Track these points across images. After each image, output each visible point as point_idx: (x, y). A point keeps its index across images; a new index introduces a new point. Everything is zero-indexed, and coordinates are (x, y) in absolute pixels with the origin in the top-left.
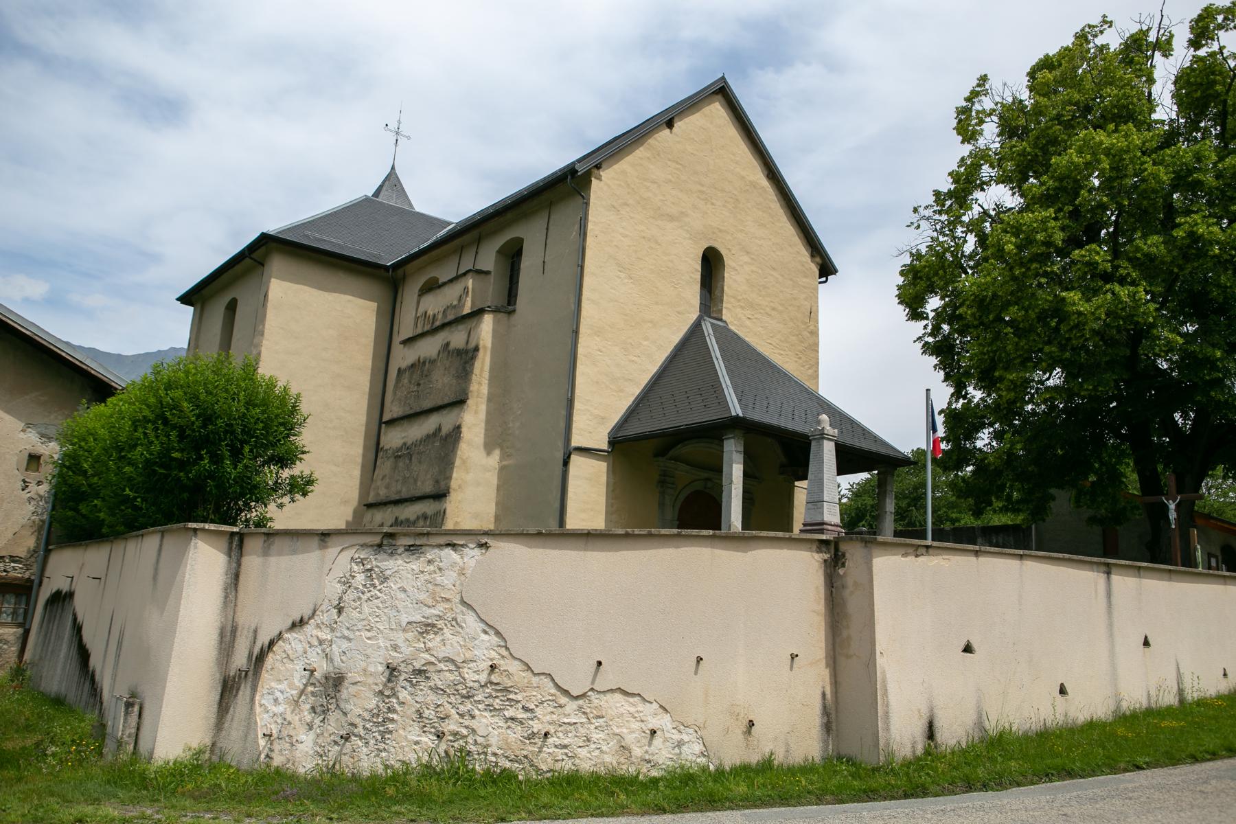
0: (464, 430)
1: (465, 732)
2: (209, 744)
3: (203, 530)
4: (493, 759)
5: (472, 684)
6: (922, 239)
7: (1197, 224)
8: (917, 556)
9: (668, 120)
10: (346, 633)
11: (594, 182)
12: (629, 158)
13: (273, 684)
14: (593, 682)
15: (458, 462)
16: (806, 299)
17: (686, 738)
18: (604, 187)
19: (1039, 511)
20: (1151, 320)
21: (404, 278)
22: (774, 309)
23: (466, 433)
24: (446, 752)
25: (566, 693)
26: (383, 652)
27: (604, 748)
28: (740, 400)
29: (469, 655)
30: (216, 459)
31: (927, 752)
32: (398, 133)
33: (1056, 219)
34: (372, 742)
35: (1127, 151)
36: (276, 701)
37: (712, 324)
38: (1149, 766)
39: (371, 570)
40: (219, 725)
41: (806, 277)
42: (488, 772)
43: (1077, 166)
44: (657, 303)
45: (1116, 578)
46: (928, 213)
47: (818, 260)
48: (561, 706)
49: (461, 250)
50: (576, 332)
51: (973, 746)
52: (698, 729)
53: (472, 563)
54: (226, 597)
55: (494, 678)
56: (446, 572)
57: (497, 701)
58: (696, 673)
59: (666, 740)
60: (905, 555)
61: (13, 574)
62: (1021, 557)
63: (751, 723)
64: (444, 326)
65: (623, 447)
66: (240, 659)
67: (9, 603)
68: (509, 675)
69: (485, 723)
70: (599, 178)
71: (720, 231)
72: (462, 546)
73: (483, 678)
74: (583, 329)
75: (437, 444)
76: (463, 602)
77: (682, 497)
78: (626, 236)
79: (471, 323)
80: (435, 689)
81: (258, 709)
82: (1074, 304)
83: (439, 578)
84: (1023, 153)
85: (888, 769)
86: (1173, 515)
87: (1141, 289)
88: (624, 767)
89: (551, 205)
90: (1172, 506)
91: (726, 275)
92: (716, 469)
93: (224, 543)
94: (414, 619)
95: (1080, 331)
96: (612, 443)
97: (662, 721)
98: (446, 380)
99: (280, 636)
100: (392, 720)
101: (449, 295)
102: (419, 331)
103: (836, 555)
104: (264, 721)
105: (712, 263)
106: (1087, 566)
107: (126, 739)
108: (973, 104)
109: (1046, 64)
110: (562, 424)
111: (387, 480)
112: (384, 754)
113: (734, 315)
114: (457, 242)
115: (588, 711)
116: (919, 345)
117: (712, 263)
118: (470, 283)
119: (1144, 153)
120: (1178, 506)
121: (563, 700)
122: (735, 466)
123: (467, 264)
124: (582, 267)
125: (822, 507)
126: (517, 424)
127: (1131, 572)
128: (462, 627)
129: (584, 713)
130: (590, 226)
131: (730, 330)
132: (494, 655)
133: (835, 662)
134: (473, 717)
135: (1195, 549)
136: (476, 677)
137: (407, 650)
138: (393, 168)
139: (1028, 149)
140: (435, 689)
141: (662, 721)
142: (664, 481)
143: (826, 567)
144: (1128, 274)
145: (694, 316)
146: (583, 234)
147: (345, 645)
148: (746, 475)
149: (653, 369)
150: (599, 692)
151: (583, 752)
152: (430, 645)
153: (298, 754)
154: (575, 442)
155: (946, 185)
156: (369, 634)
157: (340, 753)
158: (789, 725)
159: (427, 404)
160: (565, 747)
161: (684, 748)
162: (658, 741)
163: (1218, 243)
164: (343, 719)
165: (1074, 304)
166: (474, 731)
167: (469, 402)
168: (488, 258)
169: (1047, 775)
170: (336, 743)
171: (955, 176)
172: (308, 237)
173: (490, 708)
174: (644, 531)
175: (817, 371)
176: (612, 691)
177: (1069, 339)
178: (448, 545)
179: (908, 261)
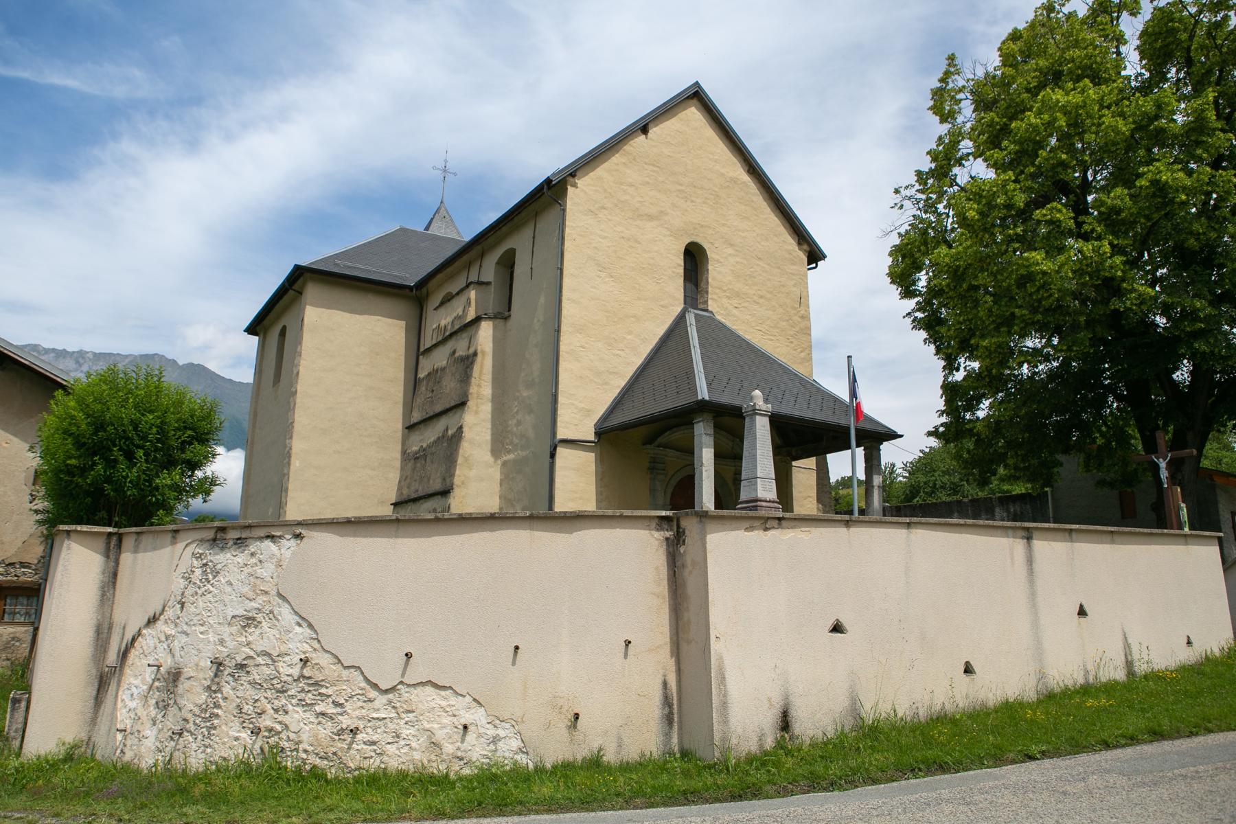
0: (465, 429)
1: (278, 727)
2: (85, 738)
3: (76, 531)
4: (304, 756)
5: (286, 678)
6: (904, 219)
7: (1160, 172)
8: (766, 529)
9: (643, 127)
10: (185, 628)
12: (606, 165)
13: (132, 680)
14: (403, 676)
15: (460, 460)
16: (794, 285)
17: (502, 733)
18: (577, 196)
19: (1043, 474)
20: (1119, 273)
21: (428, 295)
23: (467, 433)
24: (262, 749)
25: (375, 686)
26: (211, 647)
27: (414, 745)
28: (709, 385)
29: (283, 648)
30: (111, 464)
31: (780, 745)
33: (1015, 181)
34: (200, 737)
35: (1084, 106)
36: (132, 694)
37: (696, 315)
38: (1044, 755)
39: (205, 565)
40: (94, 721)
42: (298, 770)
43: (1035, 128)
44: (639, 299)
45: (1039, 545)
46: (908, 193)
47: (805, 247)
48: (370, 701)
49: (469, 265)
50: (558, 331)
51: (842, 736)
52: (515, 723)
53: (288, 554)
54: (103, 595)
55: (306, 672)
56: (266, 565)
57: (310, 695)
58: (514, 664)
59: (480, 736)
60: (751, 529)
61: (23, 578)
62: (909, 525)
63: (577, 716)
66: (112, 658)
67: (22, 604)
68: (321, 668)
69: (297, 718)
70: (575, 185)
72: (280, 537)
73: (296, 671)
74: (564, 328)
76: (280, 595)
77: (674, 482)
78: (605, 238)
79: (470, 331)
80: (253, 683)
81: (120, 704)
82: (1038, 264)
83: (259, 571)
84: (991, 124)
85: (721, 767)
86: (1164, 474)
87: (1106, 243)
88: (435, 765)
89: (536, 215)
90: (1163, 464)
92: (689, 451)
93: (101, 543)
94: (237, 613)
95: (1047, 291)
96: (603, 432)
97: (477, 716)
98: (453, 385)
99: (139, 633)
100: (217, 716)
101: (456, 308)
102: (434, 342)
103: (678, 532)
104: (123, 719)
105: (694, 258)
106: (999, 532)
107: (12, 734)
108: (947, 84)
109: (1015, 36)
112: (209, 750)
113: (719, 304)
114: (465, 258)
115: (398, 705)
116: (909, 320)
117: (694, 258)
118: (473, 294)
119: (1102, 107)
120: (1169, 465)
121: (373, 694)
122: (704, 450)
124: (561, 270)
126: (515, 421)
127: (1060, 535)
128: (277, 620)
129: (394, 707)
130: (567, 231)
131: (715, 320)
132: (306, 647)
133: (678, 648)
134: (287, 713)
135: (1179, 508)
136: (290, 671)
137: (231, 644)
139: (997, 119)
140: (253, 683)
141: (477, 716)
143: (668, 545)
144: (1093, 230)
145: (679, 308)
147: (184, 639)
148: (717, 456)
149: (638, 361)
150: (409, 686)
151: (391, 749)
152: (250, 638)
153: (143, 749)
154: (560, 436)
155: (927, 165)
156: (202, 629)
157: (175, 749)
158: (621, 714)
159: (438, 409)
160: (374, 743)
161: (500, 744)
162: (471, 737)
163: (1184, 188)
164: (179, 714)
165: (1038, 264)
166: (287, 727)
168: (489, 269)
169: (913, 770)
170: (172, 739)
171: (934, 155)
172: (338, 265)
173: (303, 704)
174: (618, 513)
176: (421, 684)
177: (1040, 301)
178: (268, 537)
179: (897, 241)
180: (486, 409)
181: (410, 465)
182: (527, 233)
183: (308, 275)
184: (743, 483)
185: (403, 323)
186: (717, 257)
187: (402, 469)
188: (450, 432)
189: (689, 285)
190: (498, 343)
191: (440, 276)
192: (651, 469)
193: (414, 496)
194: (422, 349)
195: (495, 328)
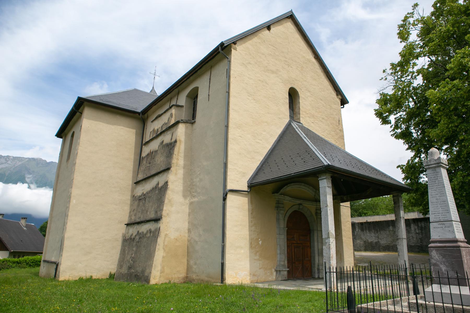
0: (169, 183)
11: (233, 51)
12: (250, 42)
15: (166, 201)
16: (336, 115)
18: (237, 54)
21: (148, 117)
22: (323, 119)
23: (170, 185)
32: (155, 75)
41: (335, 104)
47: (340, 97)
49: (171, 99)
50: (227, 127)
64: (161, 133)
65: (256, 188)
70: (235, 49)
71: (296, 80)
74: (231, 125)
75: (157, 192)
77: (288, 215)
78: (251, 79)
89: (211, 67)
91: (300, 101)
101: (164, 119)
102: (151, 138)
105: (293, 95)
110: (222, 177)
111: (135, 212)
114: (169, 96)
117: (293, 95)
123: (174, 102)
124: (228, 93)
126: (198, 179)
130: (232, 72)
138: (153, 88)
142: (279, 206)
146: (229, 77)
149: (269, 146)
159: (153, 172)
167: (172, 169)
168: (182, 100)
180: (181, 172)
181: (136, 203)
182: (205, 78)
183: (85, 103)
184: (432, 225)
185: (135, 130)
187: (131, 205)
188: (160, 186)
190: (189, 136)
191: (154, 107)
192: (277, 207)
193: (138, 220)
194: (144, 142)
195: (187, 128)
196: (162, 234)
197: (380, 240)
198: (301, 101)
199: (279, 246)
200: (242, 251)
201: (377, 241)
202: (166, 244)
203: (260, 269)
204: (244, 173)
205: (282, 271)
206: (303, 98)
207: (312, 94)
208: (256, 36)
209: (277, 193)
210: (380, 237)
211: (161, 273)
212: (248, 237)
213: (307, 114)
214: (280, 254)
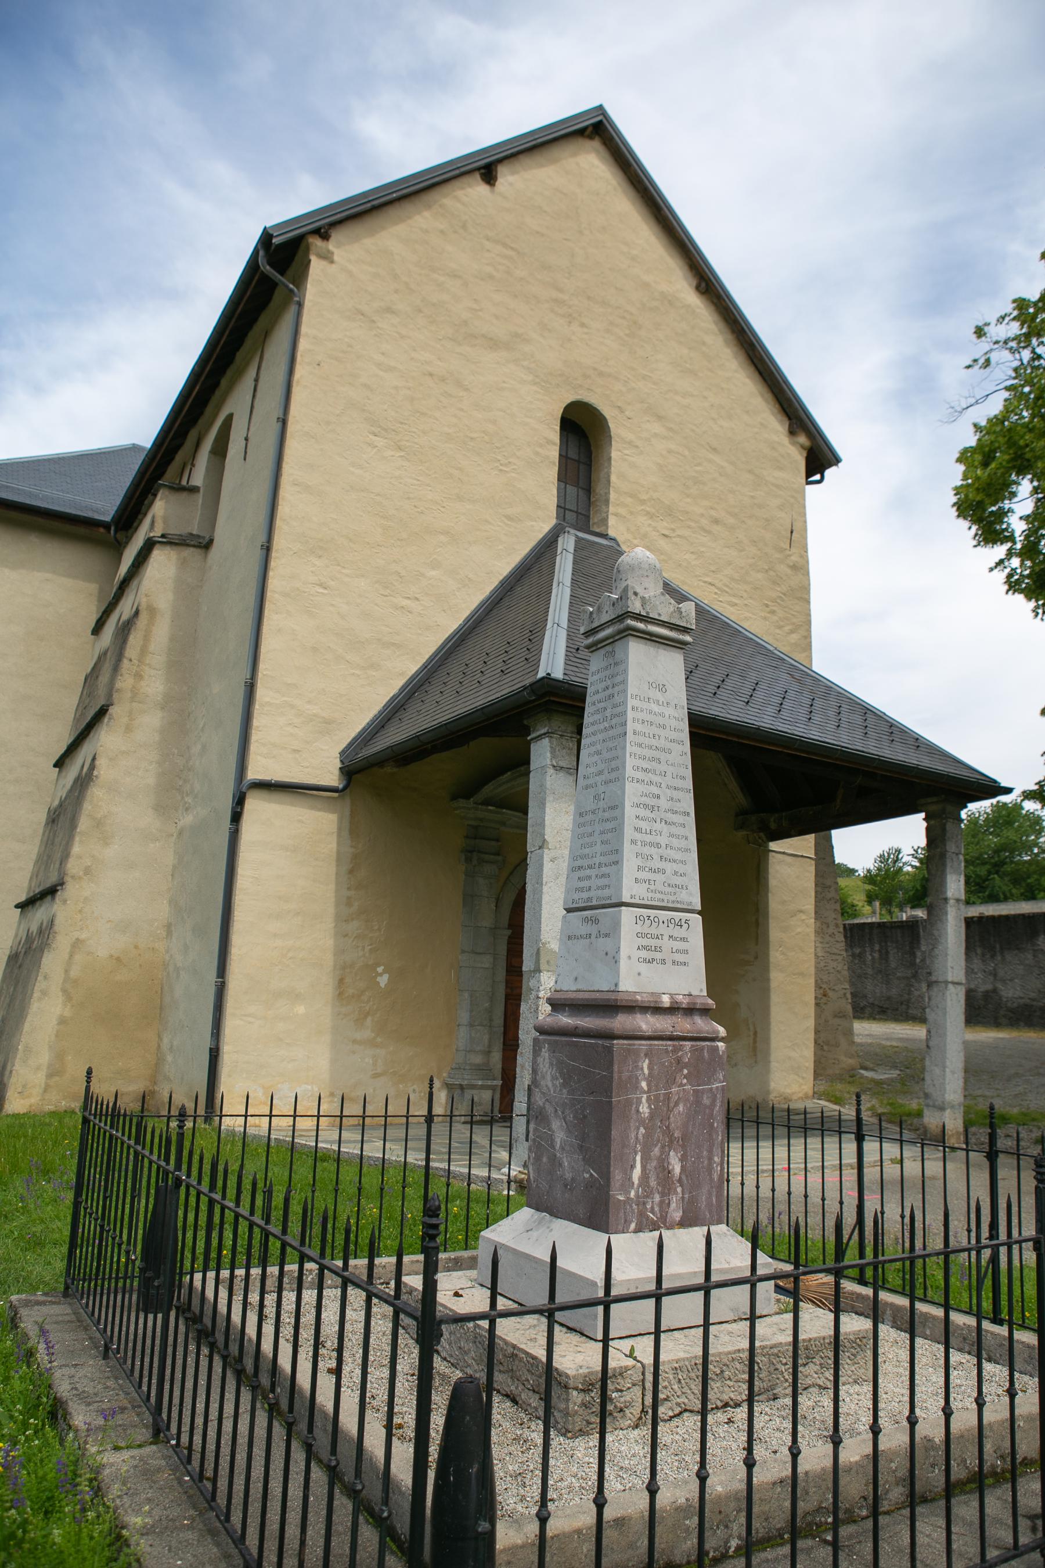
11: (316, 266)
16: (781, 507)
22: (716, 521)
37: (579, 540)
41: (781, 468)
47: (803, 439)
70: (328, 257)
71: (601, 374)
91: (614, 454)
105: (582, 433)
116: (1001, 576)
117: (582, 433)
124: (284, 422)
125: (613, 932)
145: (544, 524)
149: (451, 623)
175: (808, 637)
180: (150, 723)
186: (630, 436)
189: (571, 490)
190: (189, 595)
192: (470, 853)
195: (183, 563)
196: (62, 943)
197: (999, 986)
198: (616, 453)
199: (466, 995)
200: (301, 1009)
201: (989, 987)
202: (74, 973)
203: (376, 1076)
204: (328, 722)
205: (473, 1087)
206: (630, 443)
207: (670, 429)
208: (429, 207)
209: (467, 797)
210: (1001, 973)
211: (50, 1076)
212: (329, 959)
213: (643, 502)
214: (471, 1025)
